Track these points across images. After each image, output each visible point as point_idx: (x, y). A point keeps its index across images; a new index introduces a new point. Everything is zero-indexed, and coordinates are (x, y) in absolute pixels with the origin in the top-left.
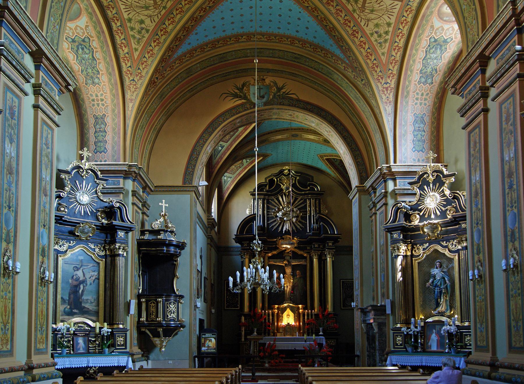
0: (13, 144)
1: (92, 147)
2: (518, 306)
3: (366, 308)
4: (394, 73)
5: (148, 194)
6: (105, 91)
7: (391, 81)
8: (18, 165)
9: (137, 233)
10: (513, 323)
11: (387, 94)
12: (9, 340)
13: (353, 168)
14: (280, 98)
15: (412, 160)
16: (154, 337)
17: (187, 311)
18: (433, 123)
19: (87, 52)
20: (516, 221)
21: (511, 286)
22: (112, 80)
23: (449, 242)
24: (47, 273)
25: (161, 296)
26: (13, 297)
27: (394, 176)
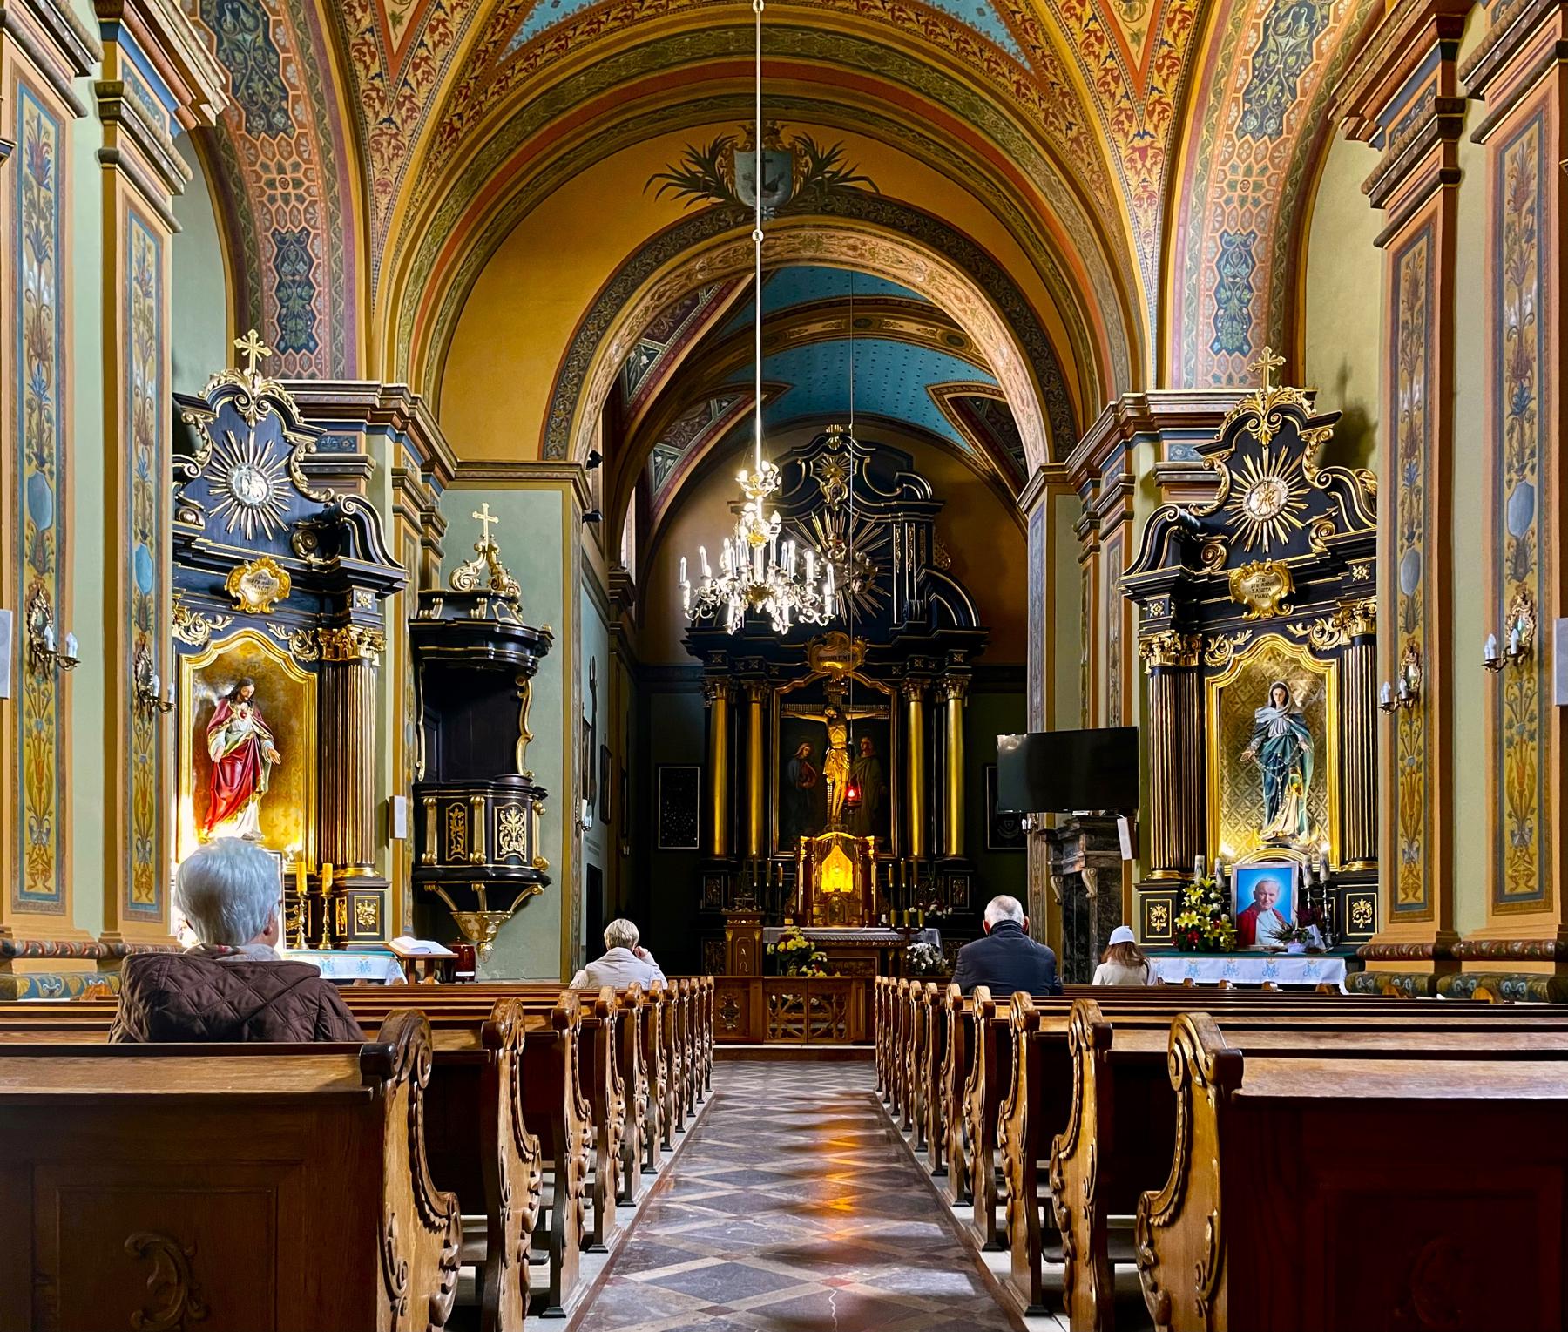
0: (46, 261)
2: (1528, 770)
3: (1062, 830)
4: (1165, 100)
5: (441, 486)
6: (306, 156)
7: (1156, 127)
8: (60, 331)
9: (409, 600)
10: (1510, 825)
11: (1144, 171)
12: (53, 863)
13: (1031, 411)
14: (822, 190)
15: (1210, 378)
16: (460, 909)
17: (555, 838)
18: (1275, 262)
19: (250, 23)
21: (1507, 713)
22: (327, 120)
23: (1314, 624)
24: (155, 680)
25: (481, 788)
26: (61, 739)
27: (1150, 427)
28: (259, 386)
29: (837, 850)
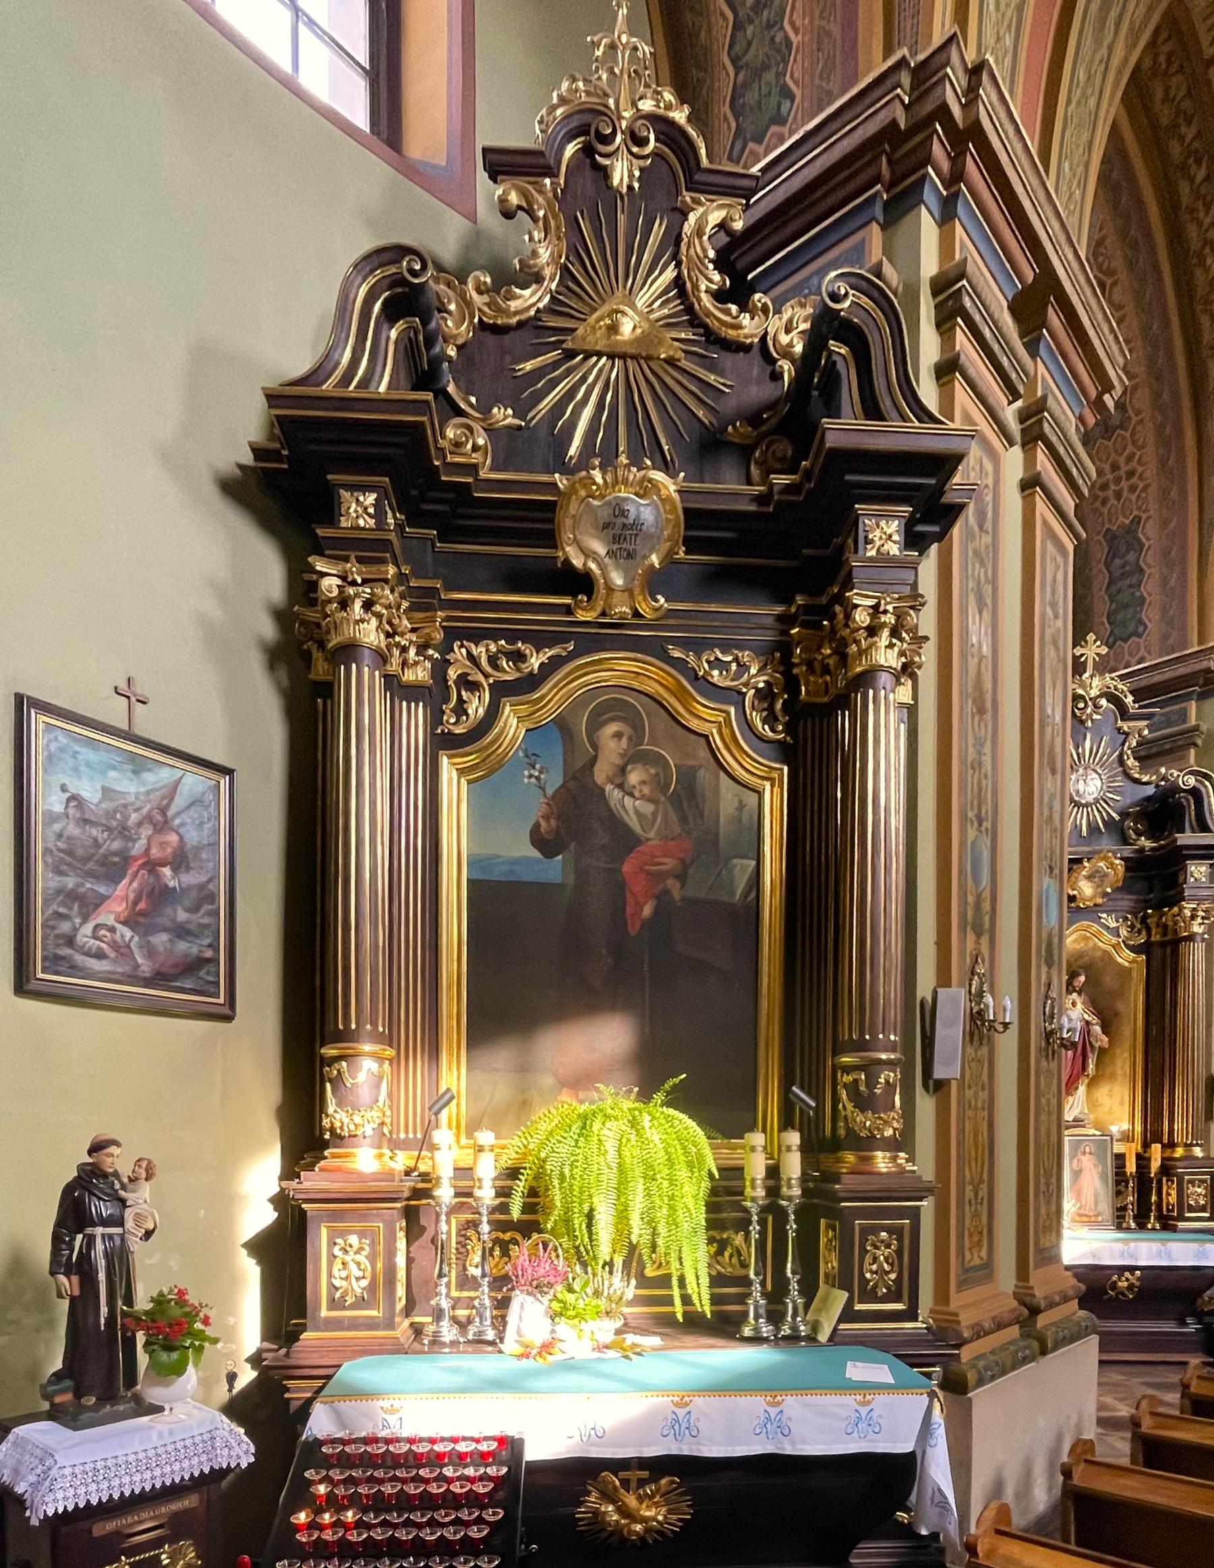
8: (995, 681)
20: (315, 1035)
28: (1095, 685)
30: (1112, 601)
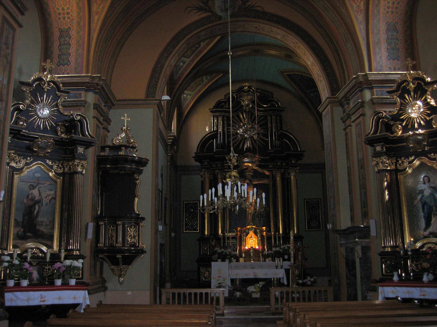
1: (56, 60)
6: (72, 5)
13: (322, 79)
15: (387, 68)
27: (369, 84)
29: (251, 233)
30: (60, 52)
